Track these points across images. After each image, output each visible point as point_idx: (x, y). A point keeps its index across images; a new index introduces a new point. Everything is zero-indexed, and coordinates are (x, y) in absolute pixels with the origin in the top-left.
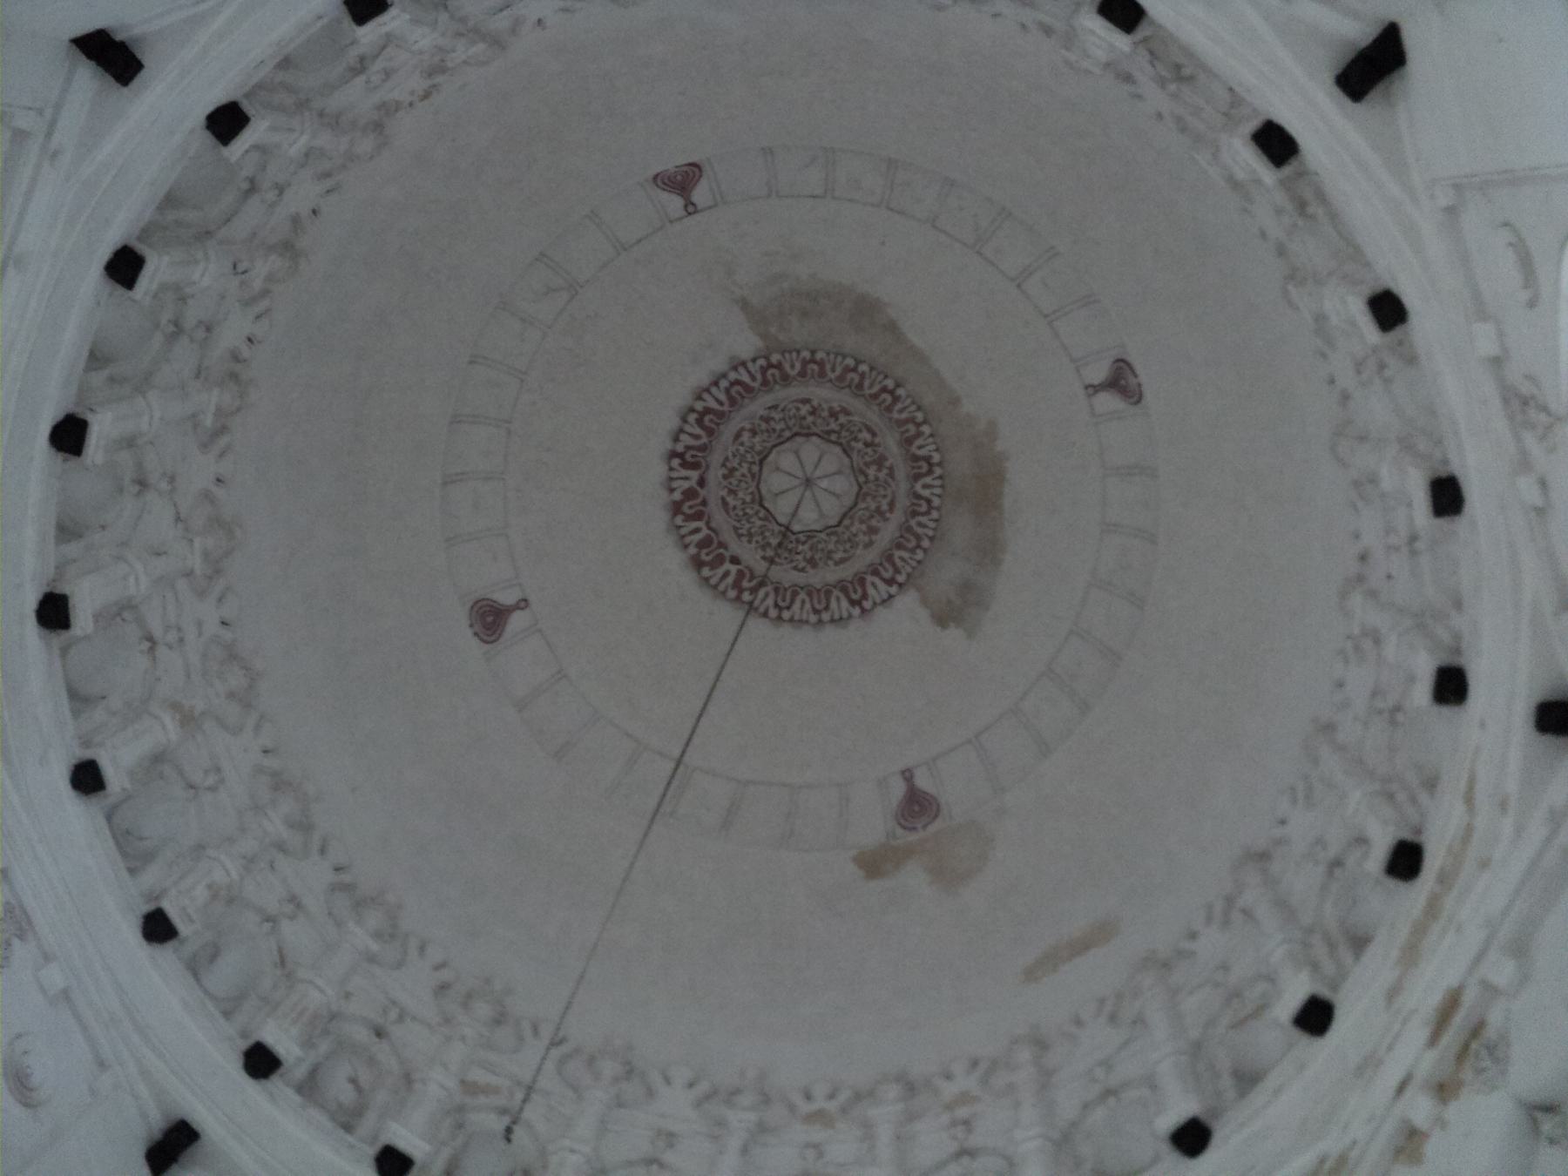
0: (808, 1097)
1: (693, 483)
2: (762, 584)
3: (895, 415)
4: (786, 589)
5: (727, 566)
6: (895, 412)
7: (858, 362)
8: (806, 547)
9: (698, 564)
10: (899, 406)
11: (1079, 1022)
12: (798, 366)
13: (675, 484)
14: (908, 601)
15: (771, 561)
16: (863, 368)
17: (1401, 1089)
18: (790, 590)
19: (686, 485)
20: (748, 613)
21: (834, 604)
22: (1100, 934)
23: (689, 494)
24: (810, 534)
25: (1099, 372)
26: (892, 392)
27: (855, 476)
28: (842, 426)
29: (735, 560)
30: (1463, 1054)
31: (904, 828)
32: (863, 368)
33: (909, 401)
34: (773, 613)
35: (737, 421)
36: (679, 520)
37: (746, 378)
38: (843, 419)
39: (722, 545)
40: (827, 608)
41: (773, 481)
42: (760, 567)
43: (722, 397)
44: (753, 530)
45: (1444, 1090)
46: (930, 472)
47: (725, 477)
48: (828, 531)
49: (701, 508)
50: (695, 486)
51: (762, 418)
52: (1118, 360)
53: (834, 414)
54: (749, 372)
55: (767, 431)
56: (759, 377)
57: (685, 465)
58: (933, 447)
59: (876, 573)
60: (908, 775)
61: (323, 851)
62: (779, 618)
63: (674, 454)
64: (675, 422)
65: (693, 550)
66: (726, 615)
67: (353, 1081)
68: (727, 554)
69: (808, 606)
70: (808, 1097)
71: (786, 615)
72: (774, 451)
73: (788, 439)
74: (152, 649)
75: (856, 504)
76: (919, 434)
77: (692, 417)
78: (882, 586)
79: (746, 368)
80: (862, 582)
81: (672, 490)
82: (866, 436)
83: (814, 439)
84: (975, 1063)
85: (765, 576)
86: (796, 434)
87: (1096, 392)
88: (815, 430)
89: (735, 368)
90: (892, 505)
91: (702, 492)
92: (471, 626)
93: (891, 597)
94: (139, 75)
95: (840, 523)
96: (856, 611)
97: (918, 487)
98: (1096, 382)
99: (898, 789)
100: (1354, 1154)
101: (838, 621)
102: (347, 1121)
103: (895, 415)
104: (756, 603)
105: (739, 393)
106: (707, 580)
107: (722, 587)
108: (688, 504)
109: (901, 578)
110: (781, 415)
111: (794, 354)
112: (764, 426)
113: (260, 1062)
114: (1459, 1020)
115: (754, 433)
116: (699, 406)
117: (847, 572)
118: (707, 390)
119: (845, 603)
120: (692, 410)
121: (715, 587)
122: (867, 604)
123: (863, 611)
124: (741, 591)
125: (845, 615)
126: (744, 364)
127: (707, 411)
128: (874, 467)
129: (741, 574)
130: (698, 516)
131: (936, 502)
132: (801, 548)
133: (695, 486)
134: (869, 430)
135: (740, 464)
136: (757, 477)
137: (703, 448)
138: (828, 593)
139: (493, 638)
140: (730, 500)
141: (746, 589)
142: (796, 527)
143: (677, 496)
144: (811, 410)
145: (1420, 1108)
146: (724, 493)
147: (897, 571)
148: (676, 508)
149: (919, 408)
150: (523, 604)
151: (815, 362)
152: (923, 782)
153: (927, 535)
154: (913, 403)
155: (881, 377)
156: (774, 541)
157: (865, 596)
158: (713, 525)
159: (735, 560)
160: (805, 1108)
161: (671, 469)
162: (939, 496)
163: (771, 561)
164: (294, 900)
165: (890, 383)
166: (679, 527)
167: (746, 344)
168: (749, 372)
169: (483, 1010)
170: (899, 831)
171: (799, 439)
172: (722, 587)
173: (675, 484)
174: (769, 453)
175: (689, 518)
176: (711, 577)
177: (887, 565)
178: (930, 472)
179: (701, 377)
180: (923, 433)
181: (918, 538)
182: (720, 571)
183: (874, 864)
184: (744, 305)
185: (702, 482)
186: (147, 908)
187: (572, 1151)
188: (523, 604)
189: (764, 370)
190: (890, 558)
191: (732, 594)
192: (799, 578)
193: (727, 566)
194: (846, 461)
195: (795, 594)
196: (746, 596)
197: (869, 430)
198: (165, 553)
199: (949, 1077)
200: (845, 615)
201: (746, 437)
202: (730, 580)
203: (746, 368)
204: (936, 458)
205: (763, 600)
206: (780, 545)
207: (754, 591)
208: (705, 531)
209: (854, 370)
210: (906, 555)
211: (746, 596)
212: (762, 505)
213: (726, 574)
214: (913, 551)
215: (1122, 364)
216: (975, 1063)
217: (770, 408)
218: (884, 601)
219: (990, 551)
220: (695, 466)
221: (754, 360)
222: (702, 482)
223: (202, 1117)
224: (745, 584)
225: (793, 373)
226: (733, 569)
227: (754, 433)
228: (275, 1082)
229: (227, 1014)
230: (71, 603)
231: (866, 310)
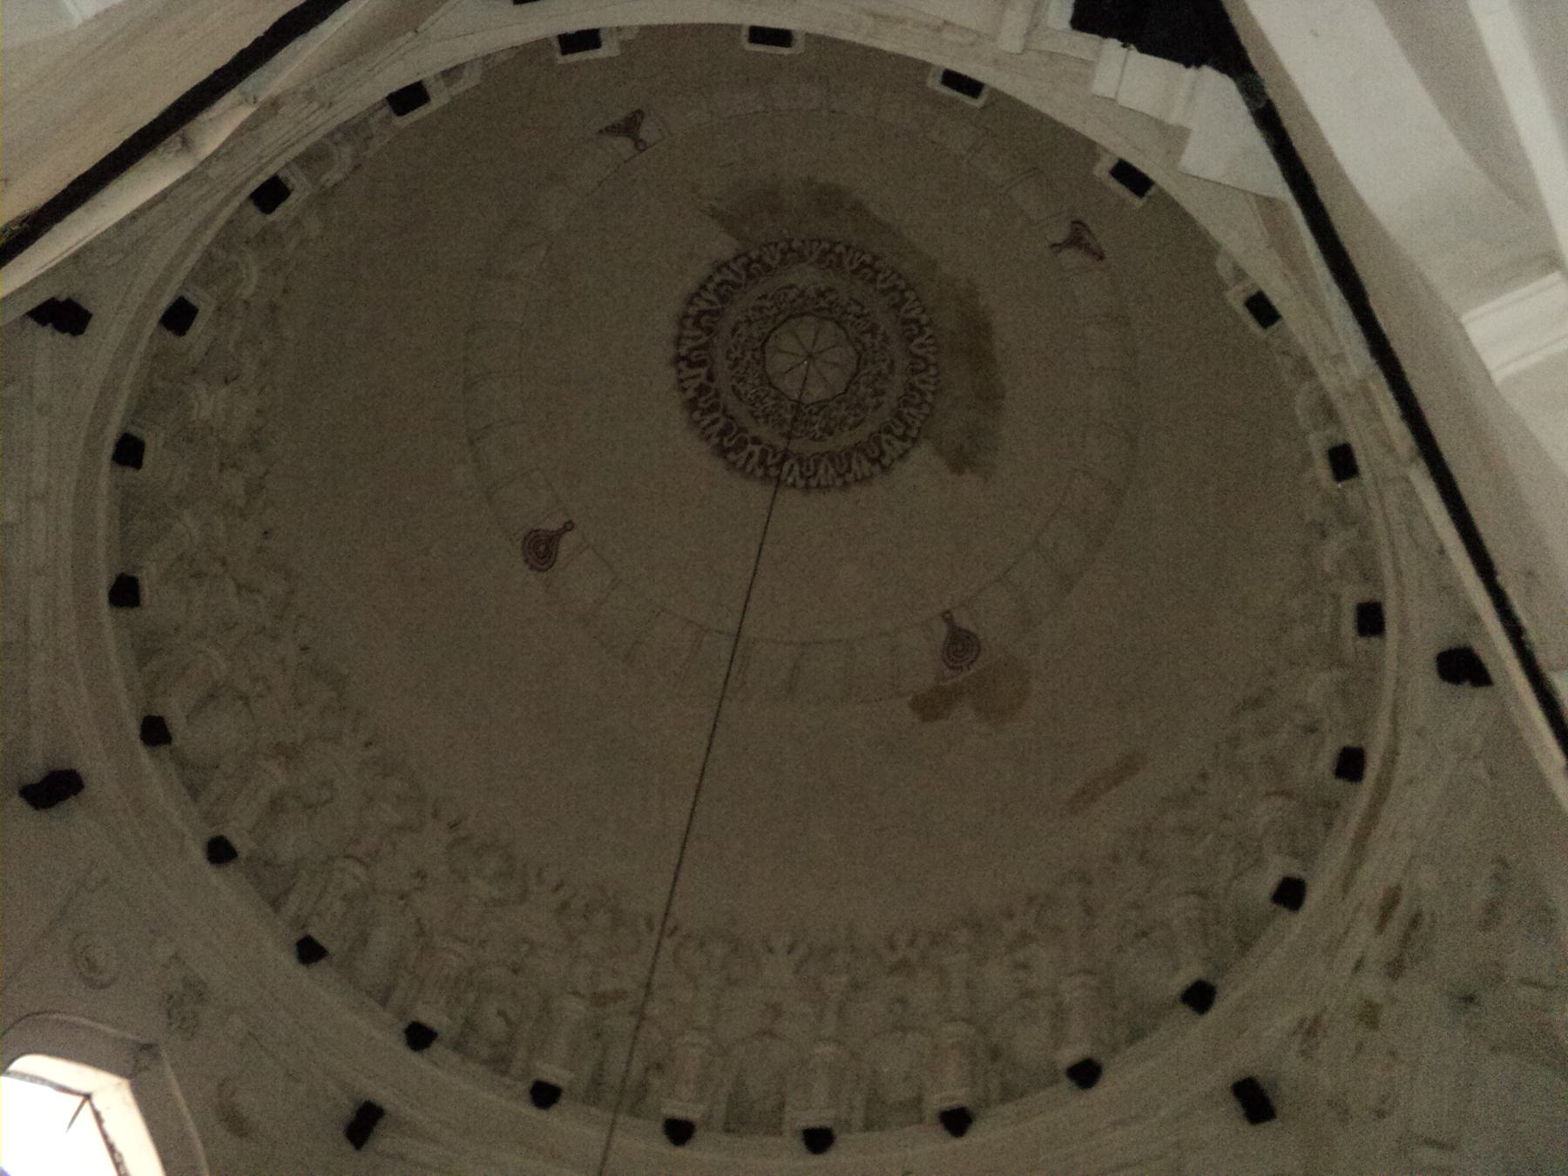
0: (892, 947)
1: (702, 379)
2: (785, 458)
3: (879, 286)
4: (808, 460)
5: (750, 447)
6: (878, 282)
7: (835, 244)
8: (820, 418)
9: (722, 452)
10: (881, 277)
11: (1115, 858)
12: (778, 257)
13: (686, 384)
14: (922, 454)
15: (789, 436)
16: (839, 249)
17: (1358, 966)
18: (812, 460)
19: (696, 382)
20: (777, 486)
21: (855, 466)
22: (1129, 766)
23: (701, 390)
24: (822, 405)
25: (1060, 233)
26: (870, 266)
27: (853, 346)
28: (831, 303)
29: (756, 441)
30: (1406, 939)
31: (952, 668)
32: (839, 249)
33: (889, 272)
34: (801, 483)
35: (733, 314)
36: (697, 415)
37: (731, 277)
38: (831, 297)
39: (742, 430)
40: (849, 470)
41: (778, 363)
42: (781, 444)
43: (713, 298)
44: (767, 411)
45: (1395, 969)
46: (921, 333)
47: (731, 368)
48: (838, 398)
49: (714, 400)
50: (705, 382)
51: (754, 309)
52: (1073, 223)
53: (821, 294)
54: (733, 271)
55: (762, 319)
56: (743, 273)
57: (691, 365)
58: (919, 310)
59: (889, 431)
60: (947, 617)
61: (435, 815)
62: (807, 487)
63: (678, 359)
64: (672, 331)
65: (715, 440)
66: (758, 493)
67: (501, 1013)
68: (748, 436)
69: (832, 471)
70: (892, 947)
71: (813, 483)
72: (773, 336)
73: (784, 321)
74: (247, 704)
75: (858, 370)
76: (904, 301)
77: (689, 322)
78: (897, 443)
79: (729, 268)
80: (877, 441)
81: (684, 390)
82: (855, 308)
83: (807, 318)
84: (1031, 900)
85: (786, 449)
86: (790, 317)
87: (946, 620)
88: (806, 309)
89: (719, 270)
90: (892, 366)
91: (713, 386)
92: (526, 561)
93: (906, 451)
94: (97, 161)
95: (846, 390)
96: (877, 468)
97: (913, 347)
98: (1060, 241)
99: (942, 630)
100: (1325, 1017)
101: (864, 480)
102: (500, 1062)
103: (879, 286)
104: (783, 477)
105: (727, 290)
106: (734, 464)
107: (749, 469)
108: (703, 399)
109: (914, 433)
110: (772, 303)
111: (772, 248)
112: (758, 316)
113: (419, 1037)
114: (1401, 910)
115: (749, 322)
116: (693, 311)
117: (861, 434)
118: (698, 294)
119: (865, 463)
120: (686, 316)
121: (743, 468)
122: (886, 461)
123: (884, 468)
124: (767, 468)
125: (867, 474)
126: (726, 264)
127: (702, 313)
128: (869, 336)
129: (764, 453)
130: (713, 408)
131: (932, 359)
132: (814, 419)
133: (705, 382)
134: (857, 303)
135: (743, 353)
136: (762, 362)
137: (705, 347)
138: (849, 456)
139: (545, 567)
140: (740, 386)
141: (771, 466)
142: (807, 399)
143: (690, 394)
144: (798, 292)
145: (1373, 986)
146: (734, 382)
147: (908, 427)
148: (692, 405)
149: (900, 277)
150: (569, 527)
151: (793, 251)
152: (964, 622)
153: (929, 391)
154: (893, 272)
155: (857, 255)
156: (789, 417)
157: (882, 453)
158: (730, 413)
159: (756, 441)
160: (892, 958)
161: (680, 371)
162: (935, 353)
163: (789, 436)
164: (421, 875)
165: (867, 259)
166: (698, 422)
167: (722, 246)
168: (733, 271)
169: (602, 919)
170: (948, 672)
171: (793, 321)
172: (749, 469)
173: (686, 384)
174: (768, 337)
175: (704, 412)
176: (737, 461)
177: (897, 422)
178: (921, 333)
179: (691, 284)
180: (907, 300)
181: (922, 393)
182: (744, 454)
183: (931, 706)
184: (714, 214)
185: (710, 377)
186: (296, 936)
187: (693, 1045)
188: (569, 527)
189: (747, 267)
190: (899, 416)
191: (760, 472)
192: (816, 447)
193: (750, 447)
194: (841, 332)
195: (817, 463)
196: (773, 472)
197: (857, 303)
198: (236, 624)
199: (1011, 916)
200: (867, 474)
201: (742, 329)
202: (755, 459)
203: (729, 268)
204: (924, 319)
205: (790, 471)
206: (795, 419)
207: (780, 465)
208: (723, 420)
209: (831, 251)
210: (913, 411)
211: (773, 472)
212: (770, 384)
213: (750, 455)
214: (918, 406)
215: (1079, 226)
216: (1031, 900)
217: (760, 298)
218: (901, 457)
219: (989, 397)
220: (702, 363)
221: (735, 259)
222: (710, 377)
223: (382, 1095)
224: (770, 461)
225: (774, 264)
226: (757, 449)
227: (749, 322)
228: (437, 1049)
229: (384, 1002)
230: (168, 722)
231: (829, 199)
